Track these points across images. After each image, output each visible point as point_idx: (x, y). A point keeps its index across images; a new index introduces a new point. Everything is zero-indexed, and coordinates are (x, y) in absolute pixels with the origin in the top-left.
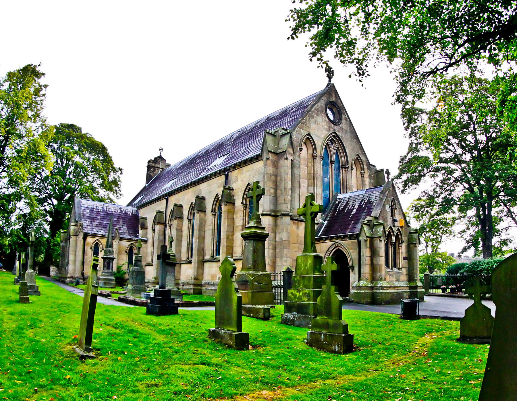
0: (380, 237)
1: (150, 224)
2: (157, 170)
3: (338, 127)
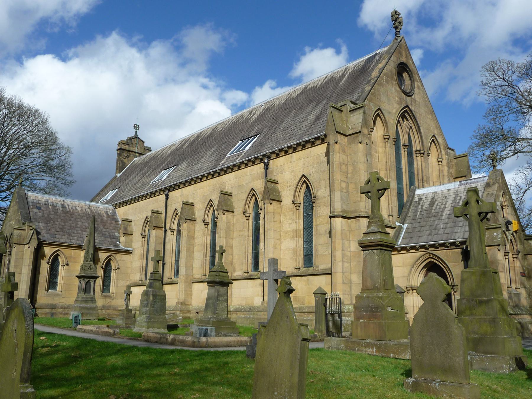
0: (499, 245)
1: (136, 228)
2: (133, 155)
3: (410, 98)
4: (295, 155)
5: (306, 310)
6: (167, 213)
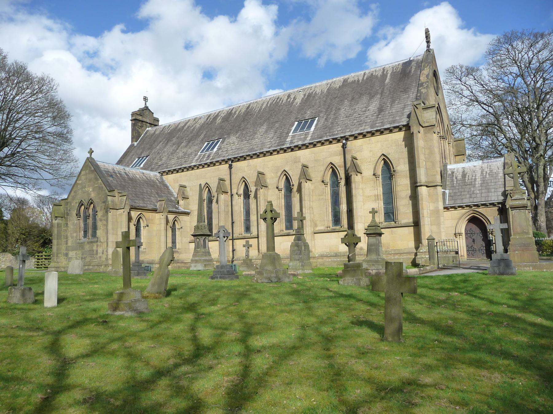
2: (146, 125)
4: (373, 138)
5: (393, 252)
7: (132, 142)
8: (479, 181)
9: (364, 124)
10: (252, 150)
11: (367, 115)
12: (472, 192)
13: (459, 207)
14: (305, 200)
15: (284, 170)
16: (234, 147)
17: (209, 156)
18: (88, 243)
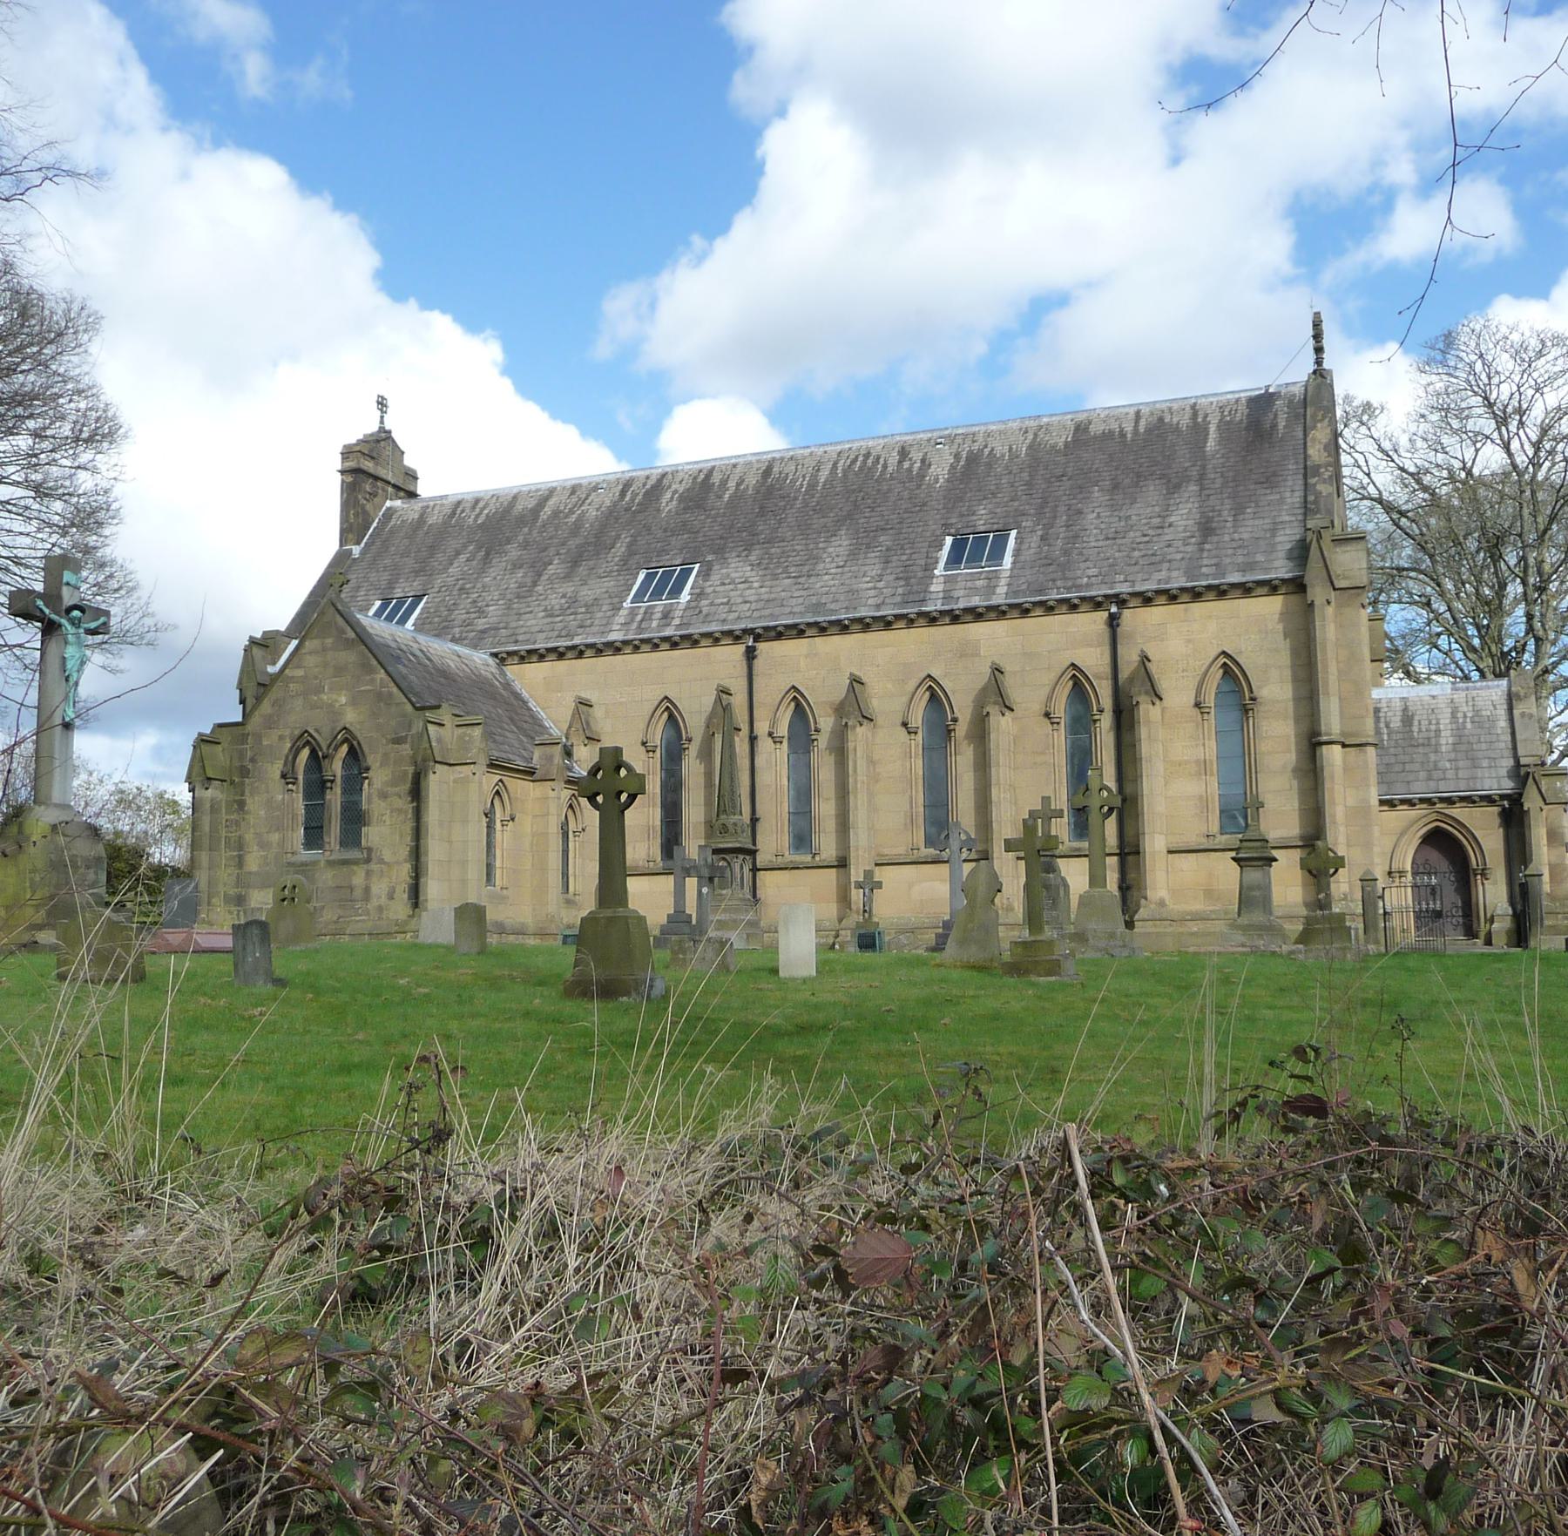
2: (383, 490)
6: (755, 694)
7: (341, 545)
8: (1446, 739)
9: (1166, 565)
10: (817, 607)
11: (1167, 538)
12: (1431, 765)
13: (1403, 802)
14: (998, 764)
15: (929, 676)
16: (750, 595)
17: (667, 615)
18: (331, 863)
